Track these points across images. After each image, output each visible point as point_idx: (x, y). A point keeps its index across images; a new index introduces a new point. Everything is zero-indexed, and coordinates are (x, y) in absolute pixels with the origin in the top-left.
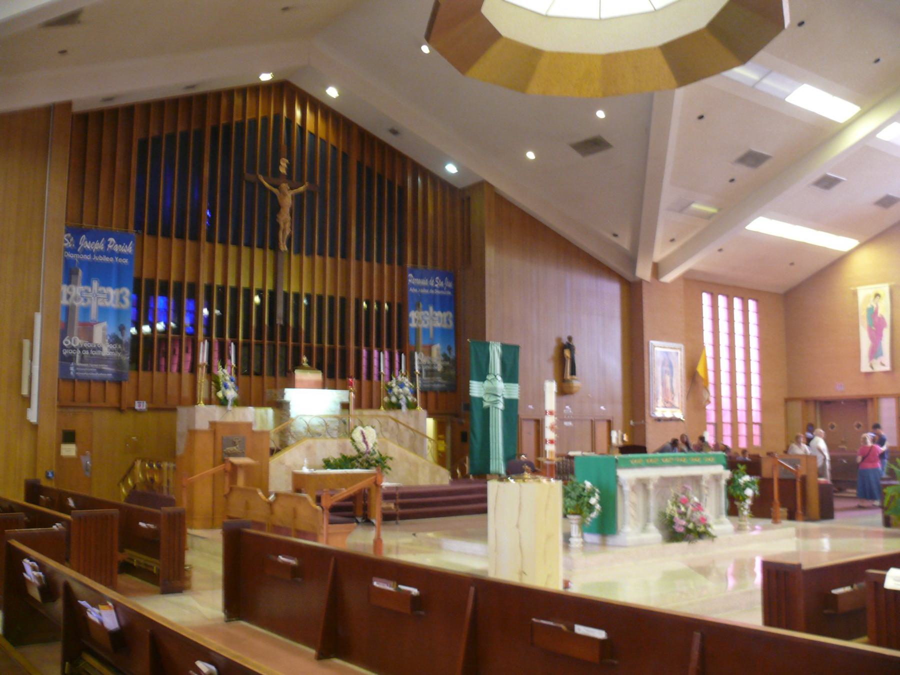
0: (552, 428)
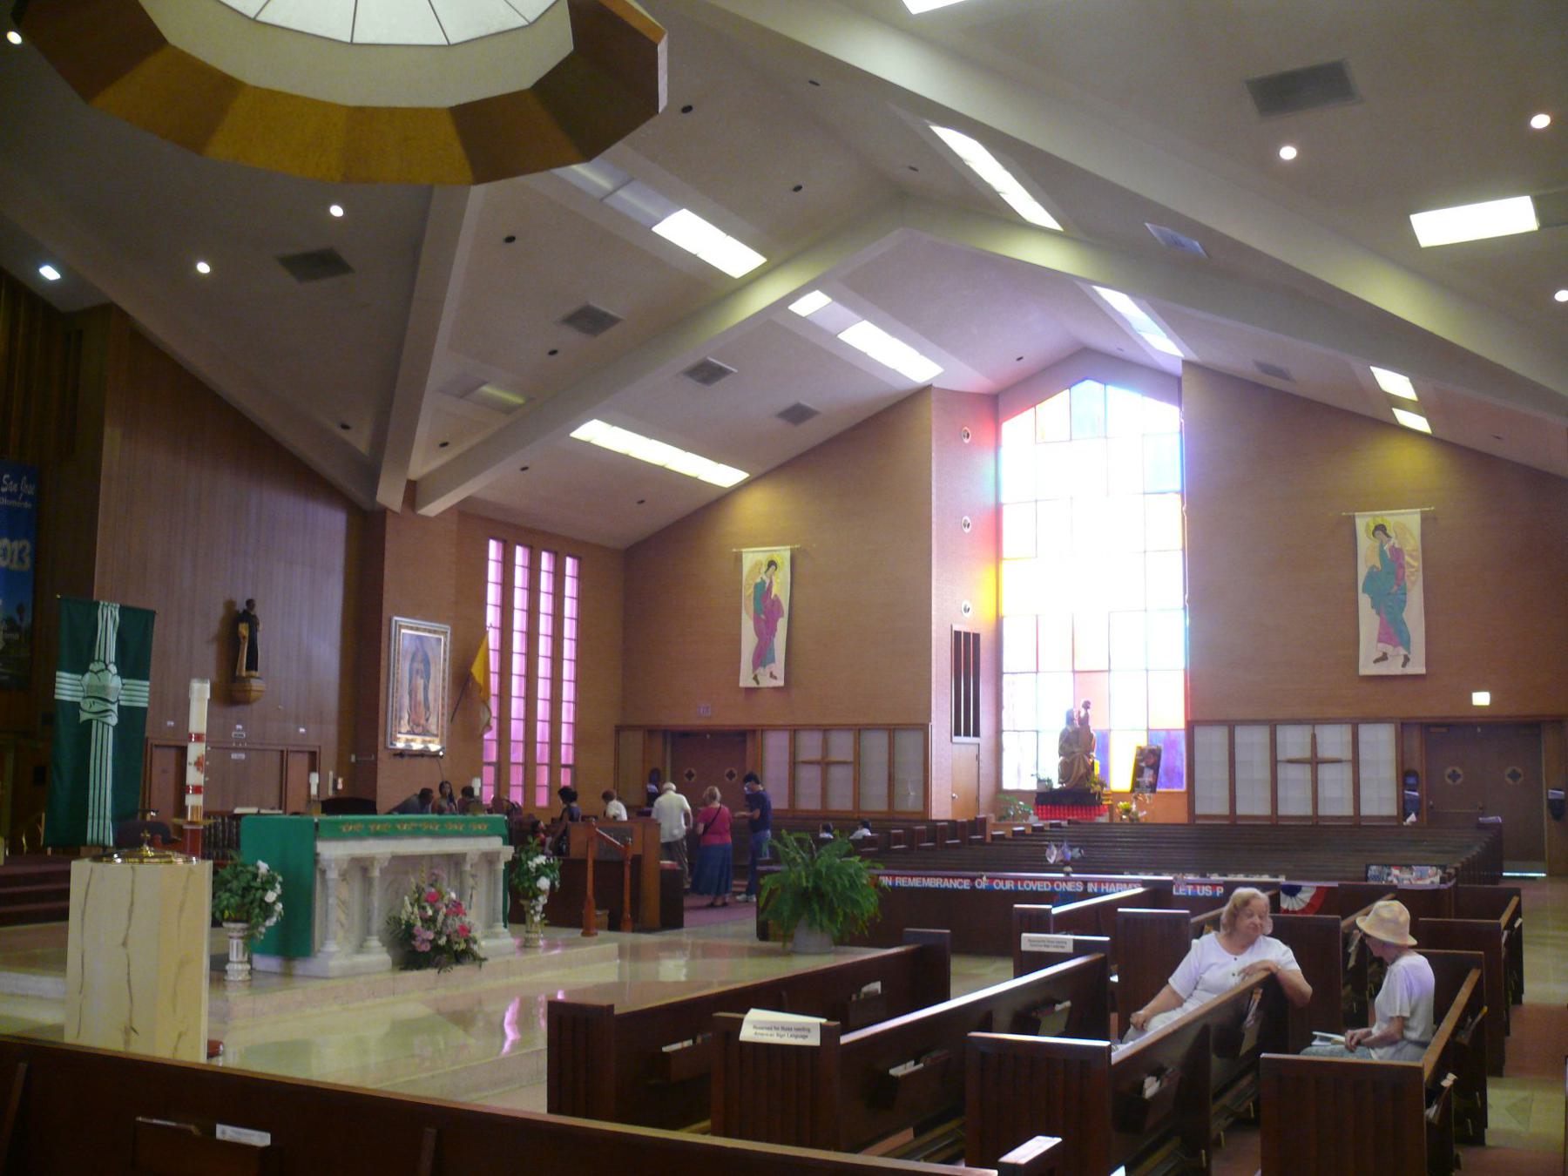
0: (198, 764)
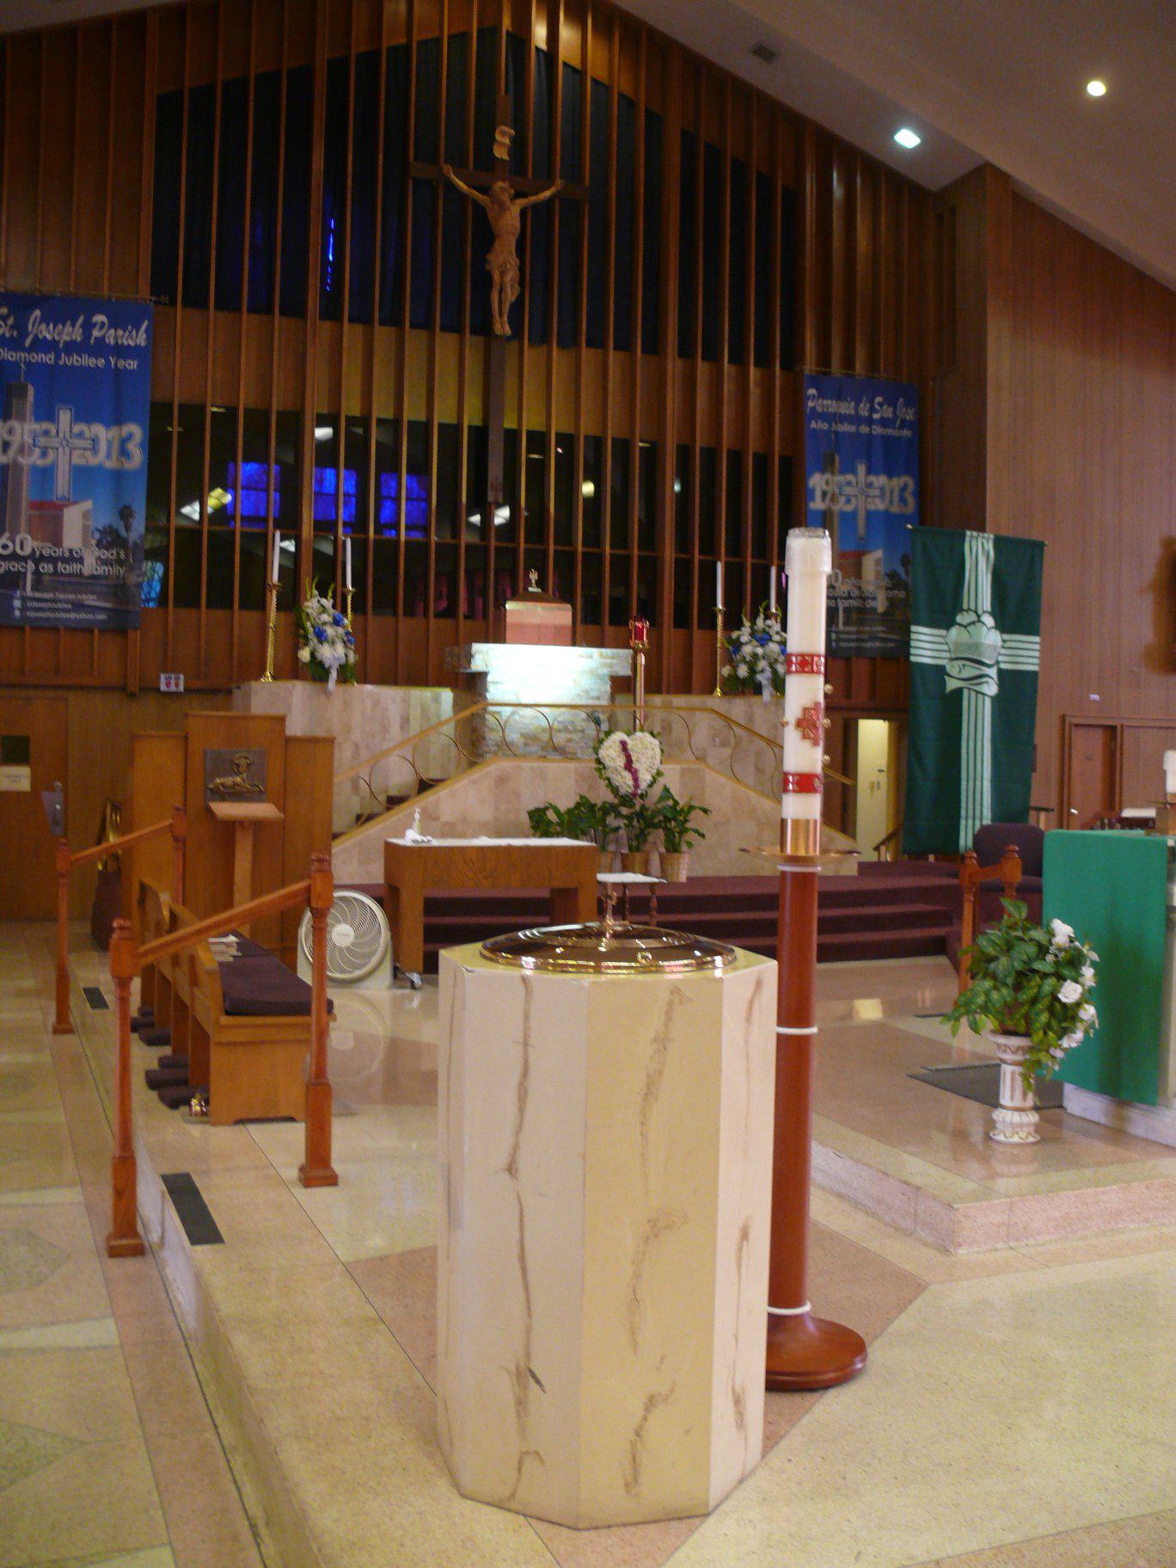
0: (805, 724)
